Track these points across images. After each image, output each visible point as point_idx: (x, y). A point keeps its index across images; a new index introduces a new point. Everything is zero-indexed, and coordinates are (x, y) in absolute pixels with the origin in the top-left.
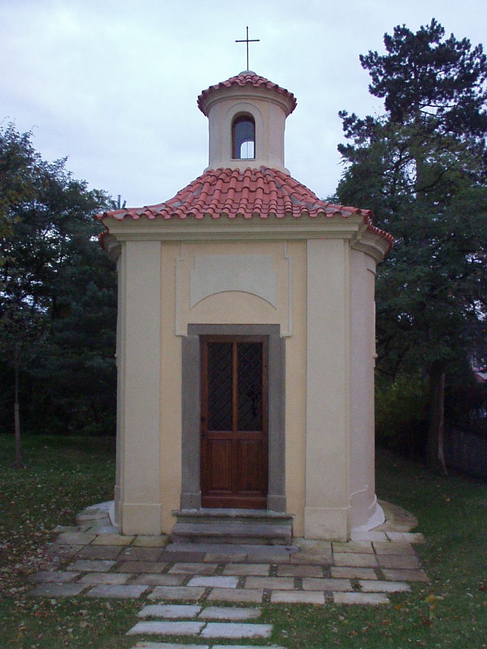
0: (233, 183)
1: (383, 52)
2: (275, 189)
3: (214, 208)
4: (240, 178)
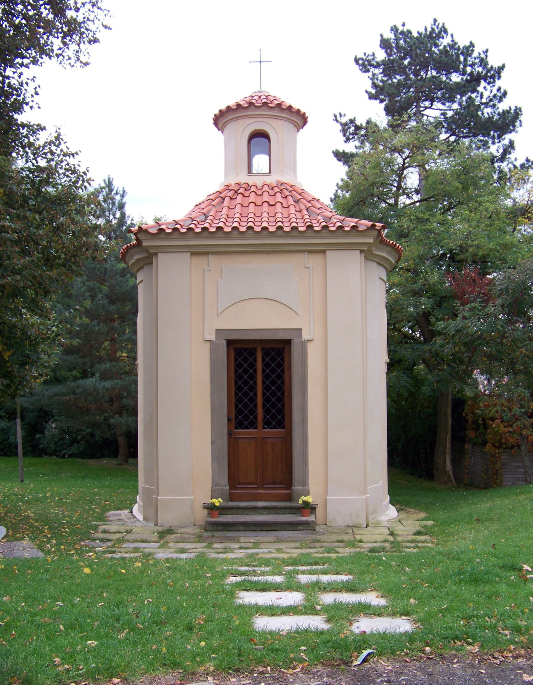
0: (253, 198)
1: (381, 55)
2: (293, 203)
3: (239, 221)
4: (259, 193)
